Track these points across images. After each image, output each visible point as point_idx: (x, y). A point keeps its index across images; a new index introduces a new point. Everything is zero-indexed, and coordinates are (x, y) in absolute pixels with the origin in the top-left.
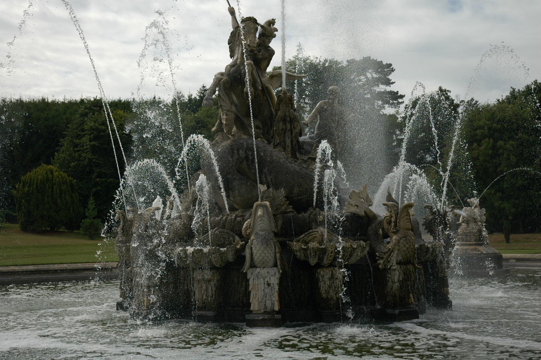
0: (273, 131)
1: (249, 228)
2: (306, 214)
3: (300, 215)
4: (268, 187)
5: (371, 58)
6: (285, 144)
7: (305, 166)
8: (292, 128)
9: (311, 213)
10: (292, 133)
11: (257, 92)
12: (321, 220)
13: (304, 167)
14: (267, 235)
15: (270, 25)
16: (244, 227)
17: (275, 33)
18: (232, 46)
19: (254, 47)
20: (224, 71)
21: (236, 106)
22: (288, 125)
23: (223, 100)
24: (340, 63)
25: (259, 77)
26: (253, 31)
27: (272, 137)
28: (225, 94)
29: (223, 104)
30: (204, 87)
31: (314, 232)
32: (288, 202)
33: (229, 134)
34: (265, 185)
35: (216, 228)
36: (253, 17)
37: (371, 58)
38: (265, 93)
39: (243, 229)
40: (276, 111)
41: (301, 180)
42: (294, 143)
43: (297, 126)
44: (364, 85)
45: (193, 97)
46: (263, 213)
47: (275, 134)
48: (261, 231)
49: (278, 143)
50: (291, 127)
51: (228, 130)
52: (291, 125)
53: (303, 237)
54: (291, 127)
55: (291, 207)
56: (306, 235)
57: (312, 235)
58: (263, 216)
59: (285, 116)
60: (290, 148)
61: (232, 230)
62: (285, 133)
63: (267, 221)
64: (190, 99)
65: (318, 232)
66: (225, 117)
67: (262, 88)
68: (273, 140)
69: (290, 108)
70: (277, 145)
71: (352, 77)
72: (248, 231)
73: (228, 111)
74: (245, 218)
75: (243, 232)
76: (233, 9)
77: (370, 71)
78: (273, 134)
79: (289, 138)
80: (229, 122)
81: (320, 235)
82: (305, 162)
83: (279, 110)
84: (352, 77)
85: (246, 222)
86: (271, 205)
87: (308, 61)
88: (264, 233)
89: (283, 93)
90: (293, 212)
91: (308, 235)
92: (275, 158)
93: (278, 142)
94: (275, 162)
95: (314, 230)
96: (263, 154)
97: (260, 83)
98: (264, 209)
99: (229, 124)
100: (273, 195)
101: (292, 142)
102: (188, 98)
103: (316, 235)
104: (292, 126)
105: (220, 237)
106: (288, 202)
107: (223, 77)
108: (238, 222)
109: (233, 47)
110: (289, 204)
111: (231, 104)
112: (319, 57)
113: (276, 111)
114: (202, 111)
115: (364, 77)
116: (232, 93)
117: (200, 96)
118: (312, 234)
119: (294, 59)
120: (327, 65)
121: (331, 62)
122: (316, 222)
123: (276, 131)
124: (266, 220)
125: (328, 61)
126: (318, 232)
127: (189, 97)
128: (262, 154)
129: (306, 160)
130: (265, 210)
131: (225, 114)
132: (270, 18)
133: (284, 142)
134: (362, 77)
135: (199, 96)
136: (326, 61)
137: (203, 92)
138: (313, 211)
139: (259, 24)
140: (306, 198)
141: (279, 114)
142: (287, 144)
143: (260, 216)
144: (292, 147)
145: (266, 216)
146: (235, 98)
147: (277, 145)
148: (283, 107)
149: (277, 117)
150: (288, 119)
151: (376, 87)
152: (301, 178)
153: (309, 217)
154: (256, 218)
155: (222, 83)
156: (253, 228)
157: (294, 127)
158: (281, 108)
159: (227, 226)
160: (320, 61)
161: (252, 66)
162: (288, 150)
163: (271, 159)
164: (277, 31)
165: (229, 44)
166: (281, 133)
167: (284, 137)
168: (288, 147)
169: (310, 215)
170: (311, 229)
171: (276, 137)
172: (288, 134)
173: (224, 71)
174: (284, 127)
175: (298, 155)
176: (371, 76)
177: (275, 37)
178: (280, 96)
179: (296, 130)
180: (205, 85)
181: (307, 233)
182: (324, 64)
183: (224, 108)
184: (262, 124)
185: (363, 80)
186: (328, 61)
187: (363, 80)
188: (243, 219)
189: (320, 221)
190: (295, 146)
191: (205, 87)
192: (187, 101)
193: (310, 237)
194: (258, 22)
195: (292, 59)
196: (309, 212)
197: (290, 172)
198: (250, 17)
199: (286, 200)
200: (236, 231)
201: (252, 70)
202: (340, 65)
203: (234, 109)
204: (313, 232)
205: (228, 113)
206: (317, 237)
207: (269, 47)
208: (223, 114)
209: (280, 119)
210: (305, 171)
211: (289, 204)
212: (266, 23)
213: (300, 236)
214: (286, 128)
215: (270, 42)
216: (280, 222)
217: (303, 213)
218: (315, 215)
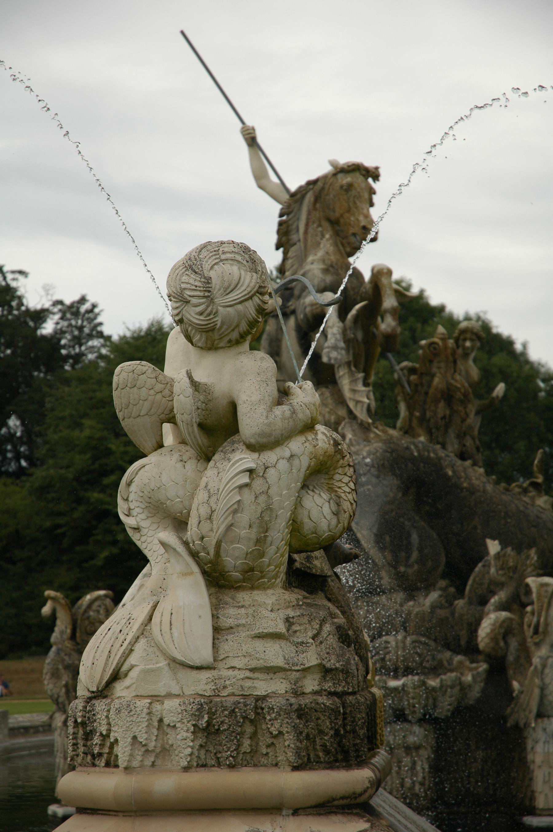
128: (450, 473)
148: (439, 368)
163: (469, 484)
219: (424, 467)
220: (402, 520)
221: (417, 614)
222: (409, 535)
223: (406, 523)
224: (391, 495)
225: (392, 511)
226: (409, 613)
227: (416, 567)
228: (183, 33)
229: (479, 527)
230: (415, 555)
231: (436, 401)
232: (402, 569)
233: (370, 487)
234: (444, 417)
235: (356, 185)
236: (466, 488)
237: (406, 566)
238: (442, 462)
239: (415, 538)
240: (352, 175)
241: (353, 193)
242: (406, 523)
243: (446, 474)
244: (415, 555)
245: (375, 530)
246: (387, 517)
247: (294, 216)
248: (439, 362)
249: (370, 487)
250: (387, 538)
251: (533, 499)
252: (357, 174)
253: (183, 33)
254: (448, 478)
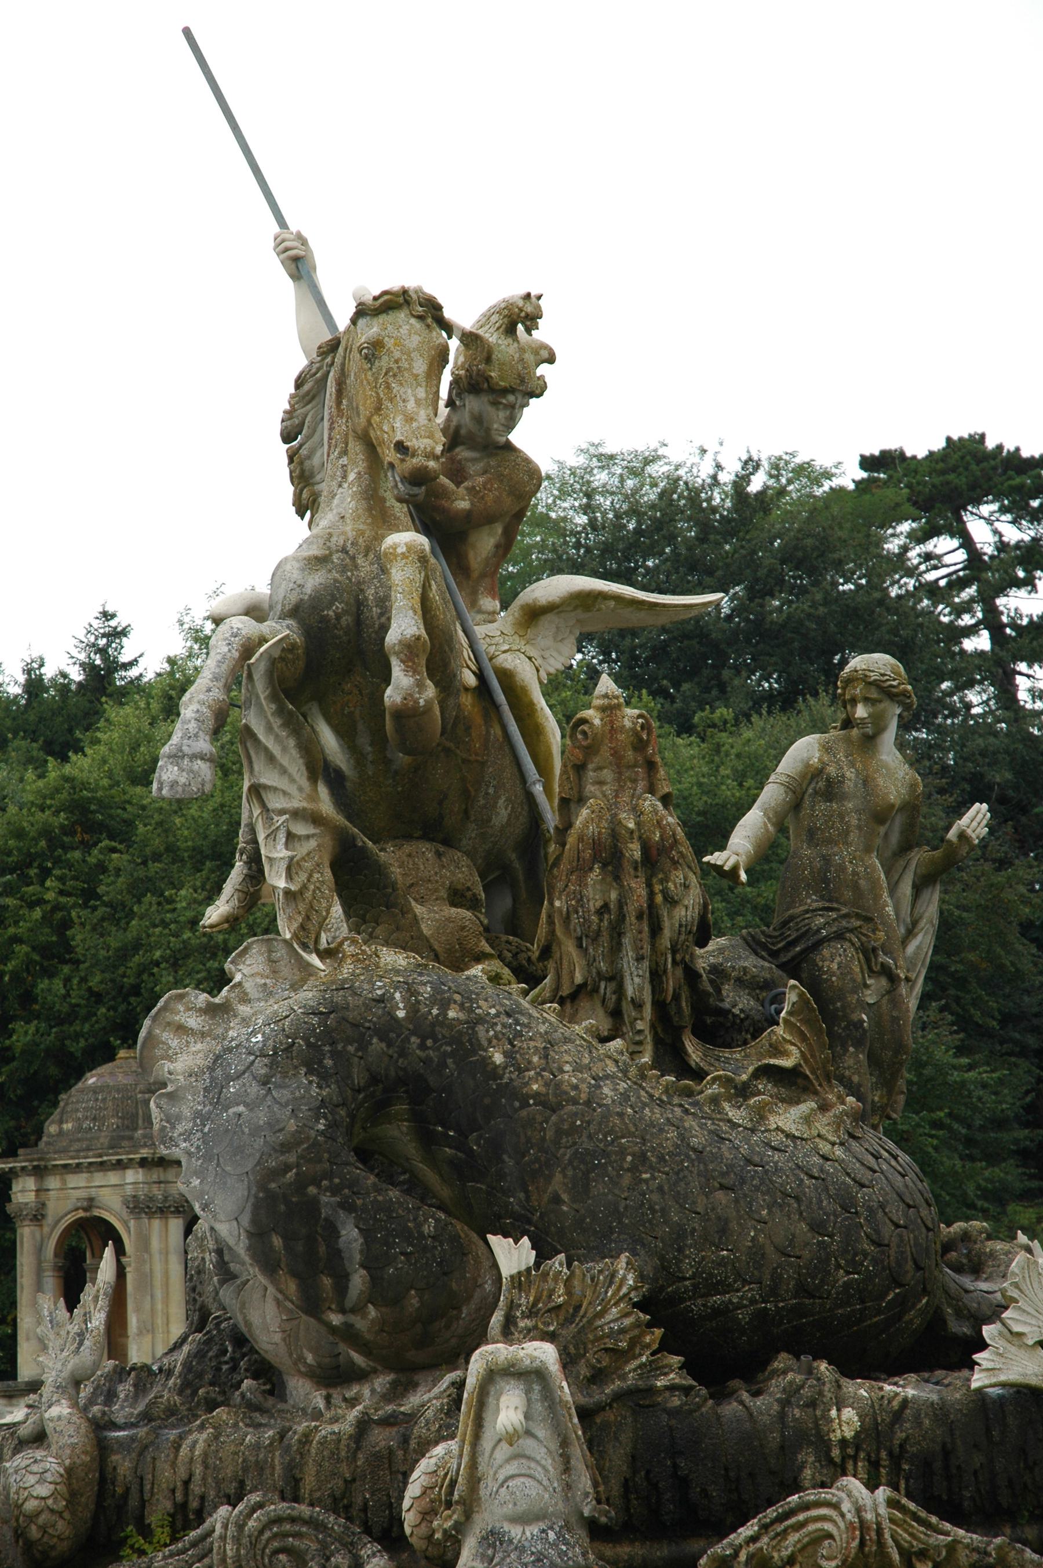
0: (550, 917)
1: (449, 1505)
2: (759, 1401)
3: (730, 1409)
4: (543, 1253)
5: (990, 444)
6: (620, 990)
7: (735, 1114)
8: (659, 899)
9: (792, 1392)
10: (656, 930)
11: (451, 702)
12: (849, 1434)
13: (734, 1126)
14: (554, 1545)
15: (510, 330)
16: (413, 1490)
17: (543, 370)
18: (303, 452)
19: (431, 455)
20: (263, 589)
21: (335, 779)
22: (638, 888)
23: (271, 758)
24: (828, 475)
25: (460, 616)
26: (420, 366)
27: (546, 952)
28: (276, 722)
29: (268, 777)
30: (107, 616)
31: (818, 1504)
32: (659, 1332)
33: (305, 946)
34: (525, 1241)
35: (255, 1498)
36: (418, 291)
37: (990, 444)
38: (496, 707)
39: (406, 1504)
40: (567, 806)
41: (720, 1195)
42: (670, 986)
43: (686, 887)
44: (958, 584)
45: (49, 672)
46: (527, 1416)
47: (559, 932)
48: (522, 1519)
49: (581, 987)
50: (651, 895)
51: (302, 927)
52: (649, 885)
53: (754, 1539)
54: (651, 895)
55: (676, 1360)
56: (765, 1527)
57: (802, 1525)
58: (528, 1433)
59: (615, 831)
60: (648, 1011)
61: (339, 1504)
62: (617, 932)
63: (548, 1463)
64: (34, 685)
65: (836, 1506)
66: (281, 852)
67: (480, 676)
68: (551, 965)
69: (641, 785)
70: (574, 996)
71: (893, 546)
72: (444, 1522)
73: (296, 814)
74: (419, 1430)
75: (409, 1519)
76: (304, 241)
77: (985, 509)
78: (552, 932)
79: (639, 959)
80: (303, 877)
81: (850, 1526)
82: (742, 1092)
83: (581, 800)
84: (893, 546)
85: (425, 1465)
86: (568, 1361)
87: (657, 470)
88: (533, 1530)
89: (603, 709)
90: (687, 1390)
91: (780, 1528)
92: (569, 1077)
93: (579, 979)
94: (575, 1102)
95: (811, 1495)
96: (506, 1054)
97: (467, 653)
98: (528, 1392)
99: (304, 887)
100: (569, 1292)
101: (656, 976)
102: (22, 678)
103: (828, 1526)
104: (658, 888)
105: (276, 1552)
106: (659, 1332)
107: (265, 628)
108: (377, 1456)
109: (309, 457)
110: (666, 1346)
111: (313, 778)
112: (712, 447)
113: (567, 806)
114: (102, 749)
115: (955, 543)
116: (314, 710)
117: (89, 668)
118: (801, 1517)
119: (581, 461)
120: (756, 484)
121: (776, 467)
122: (822, 1444)
123: (567, 920)
124: (540, 1452)
125: (765, 464)
126: (836, 1506)
127: (28, 671)
128: (498, 1058)
129: (746, 1085)
130: (536, 1395)
131: (282, 837)
132: (512, 290)
133: (616, 978)
134: (943, 544)
135: (82, 665)
136: (751, 465)
137: (102, 642)
138: (799, 1378)
139: (447, 327)
140: (753, 1301)
141: (578, 823)
142: (630, 991)
143: (511, 1438)
144: (659, 1006)
145: (541, 1433)
146: (328, 739)
147: (574, 996)
148: (601, 783)
149: (571, 840)
150: (634, 850)
151: (1023, 592)
152: (722, 1187)
153: (782, 1416)
154: (487, 1443)
155: (262, 667)
156: (470, 1506)
157: (665, 893)
158: (590, 788)
159: (309, 1482)
160: (719, 467)
161: (423, 560)
162: (640, 1025)
163: (547, 1084)
164: (551, 359)
165: (287, 437)
166: (598, 933)
167: (616, 948)
168: (638, 1006)
169: (785, 1403)
170: (797, 1487)
171: (569, 947)
172: (634, 932)
173: (263, 589)
174: (614, 895)
175: (694, 1051)
176: (992, 539)
177: (539, 395)
178: (584, 721)
179: (680, 913)
180: (110, 609)
181: (771, 1513)
182: (741, 482)
183: (275, 802)
184: (482, 876)
185: (947, 559)
186: (765, 464)
187: (947, 559)
188: (405, 1440)
189: (843, 1442)
190: (676, 997)
191: (113, 616)
192: (17, 690)
193: (793, 1538)
194: (448, 314)
195: (577, 461)
196: (776, 1387)
197: (661, 1159)
198: (405, 292)
199: (650, 1325)
200: (365, 1509)
201: (425, 588)
202: (827, 485)
203: (326, 805)
204: (806, 1507)
205: (301, 829)
206: (830, 1536)
207: (509, 447)
208: (272, 836)
209: (588, 854)
210: (745, 1149)
211: (666, 1346)
212: (487, 317)
213: (734, 1529)
214: (621, 904)
215: (511, 423)
216: (618, 1456)
217: (745, 1396)
218: (812, 1404)
219: (423, 1046)
220: (312, 1190)
221: (323, 1442)
222: (332, 1231)
223: (325, 1199)
224: (292, 1125)
225: (287, 1168)
226: (306, 1438)
227: (372, 1312)
228: (187, 33)
229: (565, 1197)
230: (358, 1281)
231: (582, 869)
232: (336, 1319)
233: (241, 1108)
234: (605, 908)
235: (389, 343)
236: (536, 1095)
237: (343, 1311)
238: (480, 1029)
239: (350, 1235)
240: (382, 318)
241: (384, 362)
242: (325, 1199)
243: (486, 1061)
244: (358, 1281)
245: (246, 1220)
246: (273, 1185)
247: (308, 438)
248: (600, 768)
249: (241, 1108)
250: (277, 1241)
251: (761, 1114)
252: (402, 315)
253: (187, 33)
254: (494, 1073)
